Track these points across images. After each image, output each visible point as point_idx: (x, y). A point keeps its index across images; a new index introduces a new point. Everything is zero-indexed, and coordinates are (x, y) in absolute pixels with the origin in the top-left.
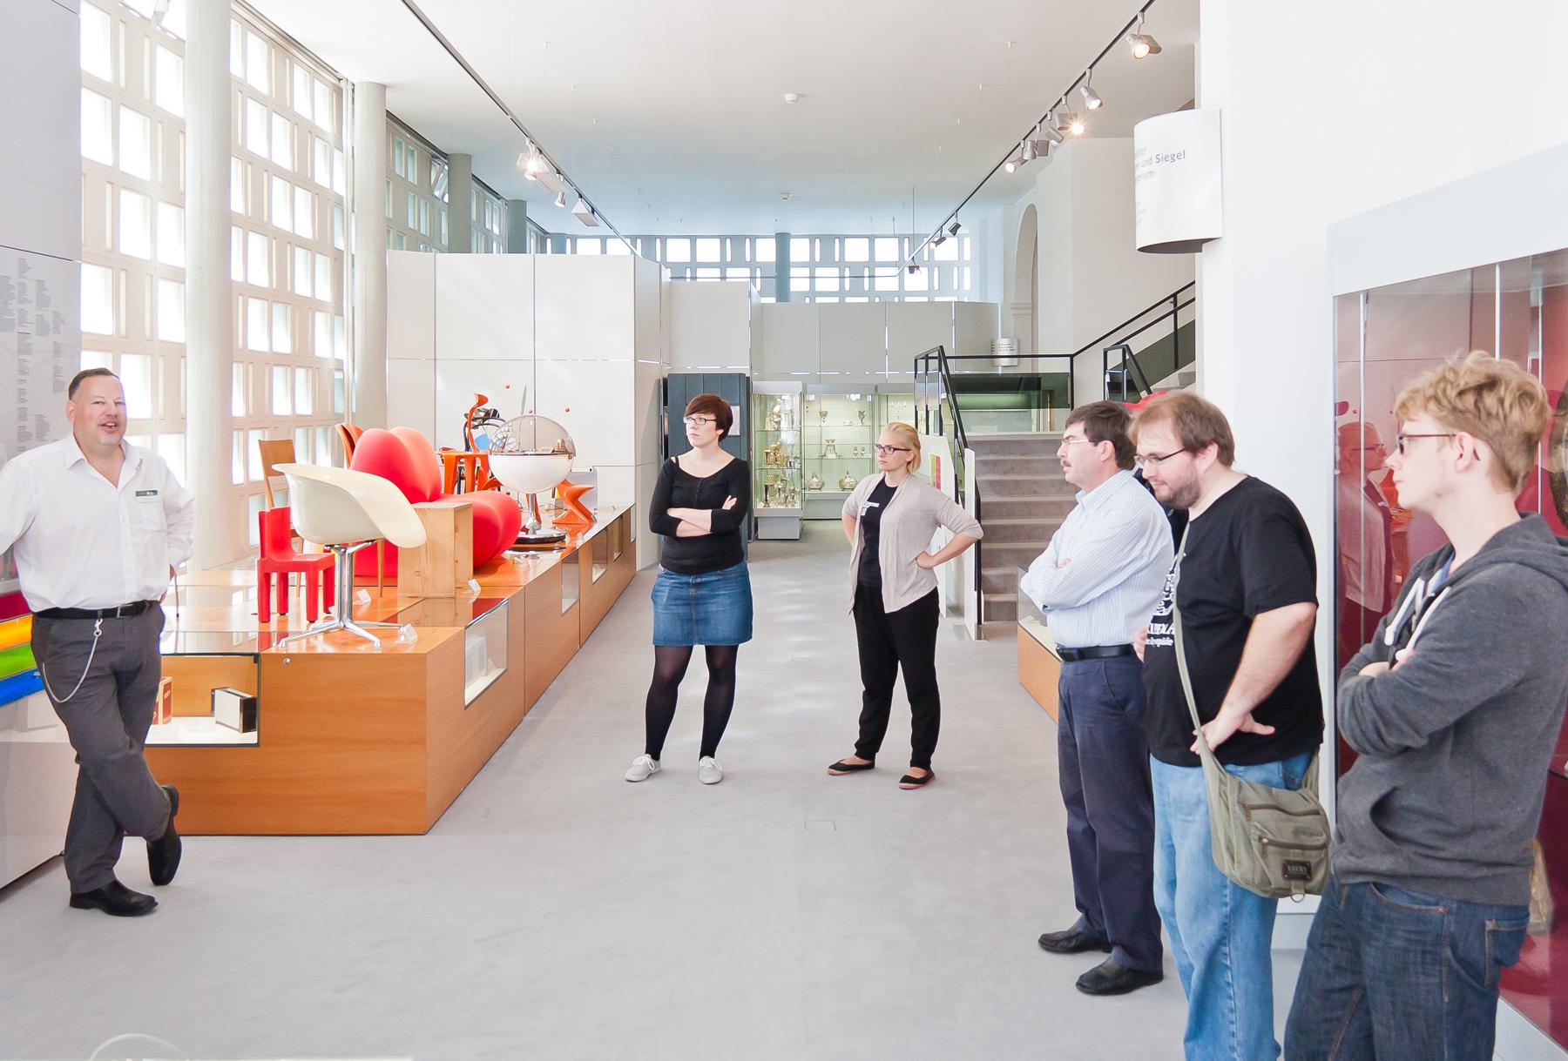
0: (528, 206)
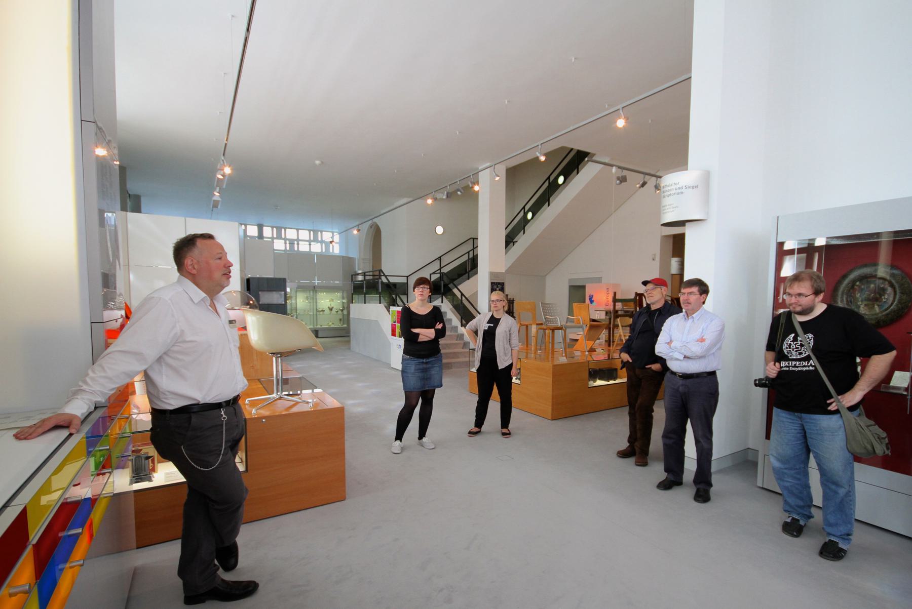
0: (143, 199)
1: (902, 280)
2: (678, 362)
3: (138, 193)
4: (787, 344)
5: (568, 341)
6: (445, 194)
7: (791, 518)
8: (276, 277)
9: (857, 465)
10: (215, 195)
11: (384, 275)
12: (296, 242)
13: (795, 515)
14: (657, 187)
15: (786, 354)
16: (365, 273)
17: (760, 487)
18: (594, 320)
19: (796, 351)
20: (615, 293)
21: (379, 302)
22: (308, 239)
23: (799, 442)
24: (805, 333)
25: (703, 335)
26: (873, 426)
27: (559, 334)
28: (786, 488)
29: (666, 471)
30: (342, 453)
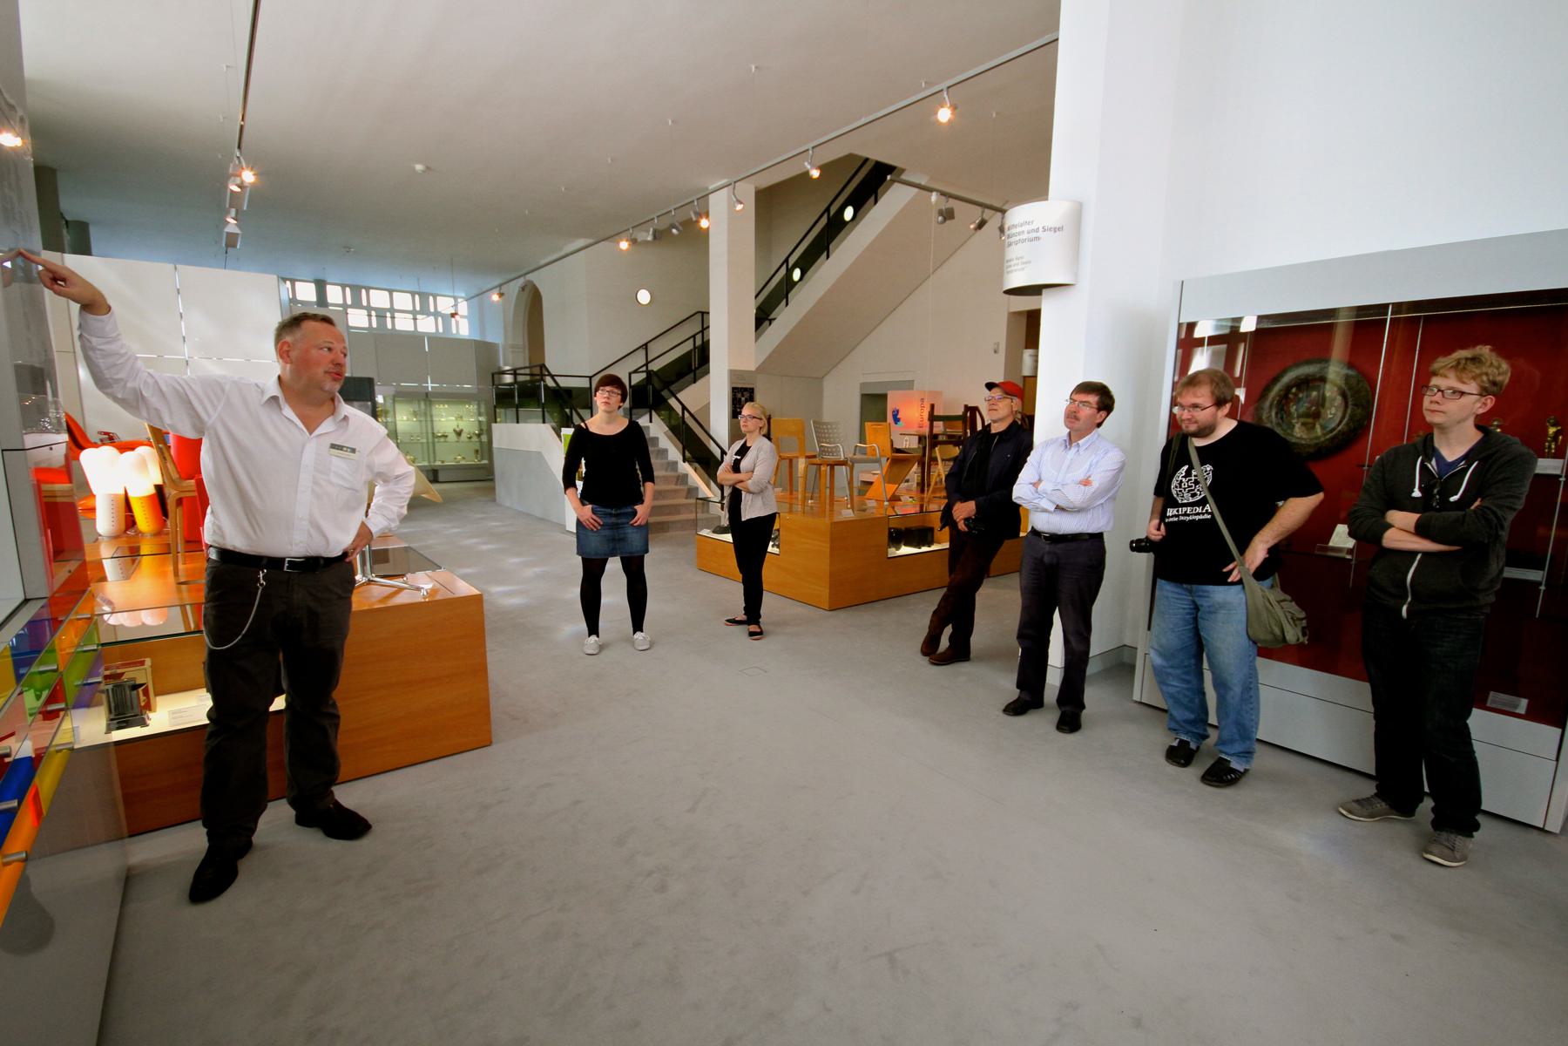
1: (1358, 384)
2: (1044, 516)
3: (83, 218)
5: (856, 484)
6: (651, 232)
8: (354, 376)
9: (1262, 663)
10: (229, 222)
11: (550, 374)
12: (388, 315)
14: (1002, 229)
17: (1136, 702)
19: (1189, 491)
20: (932, 406)
21: (541, 420)
24: (1203, 464)
25: (1090, 473)
27: (841, 471)
28: (1172, 696)
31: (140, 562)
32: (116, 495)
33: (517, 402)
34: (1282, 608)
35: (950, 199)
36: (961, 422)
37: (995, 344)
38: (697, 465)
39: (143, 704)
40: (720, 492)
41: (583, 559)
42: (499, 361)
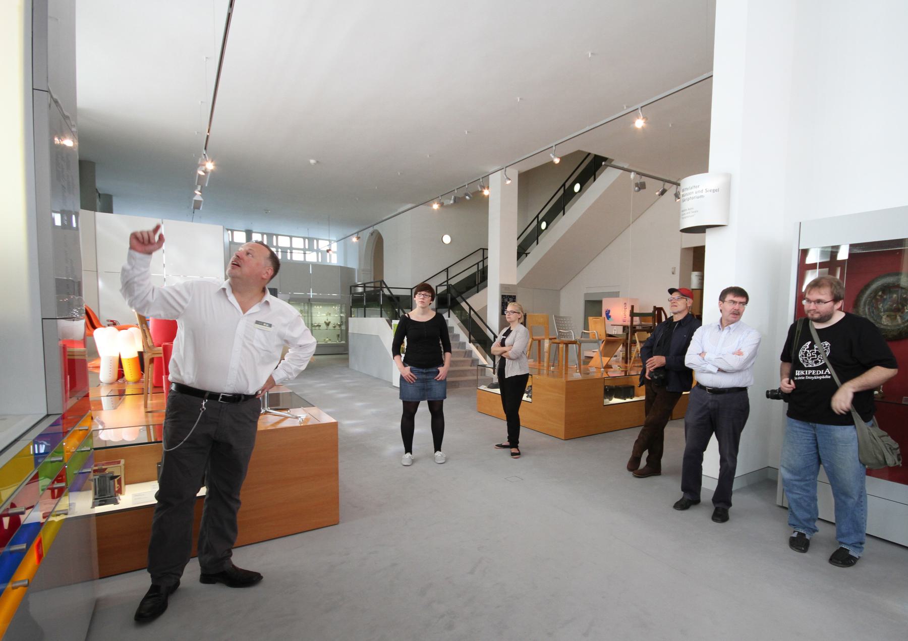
2: (710, 375)
3: (111, 193)
4: (803, 352)
5: (582, 358)
7: (796, 533)
9: (868, 478)
10: (196, 194)
11: (387, 287)
12: (289, 251)
13: (801, 529)
14: (677, 196)
15: (802, 362)
16: (364, 284)
18: (610, 336)
19: (812, 359)
20: (633, 307)
21: (380, 316)
22: (302, 247)
23: (811, 453)
26: (886, 437)
27: (573, 348)
28: (795, 501)
29: (683, 490)
30: (336, 472)
31: (124, 399)
32: (114, 357)
33: (365, 304)
34: (883, 441)
35: (643, 177)
36: (651, 317)
37: (673, 268)
38: (478, 345)
39: (117, 489)
40: (493, 362)
41: (404, 402)
42: (354, 277)
